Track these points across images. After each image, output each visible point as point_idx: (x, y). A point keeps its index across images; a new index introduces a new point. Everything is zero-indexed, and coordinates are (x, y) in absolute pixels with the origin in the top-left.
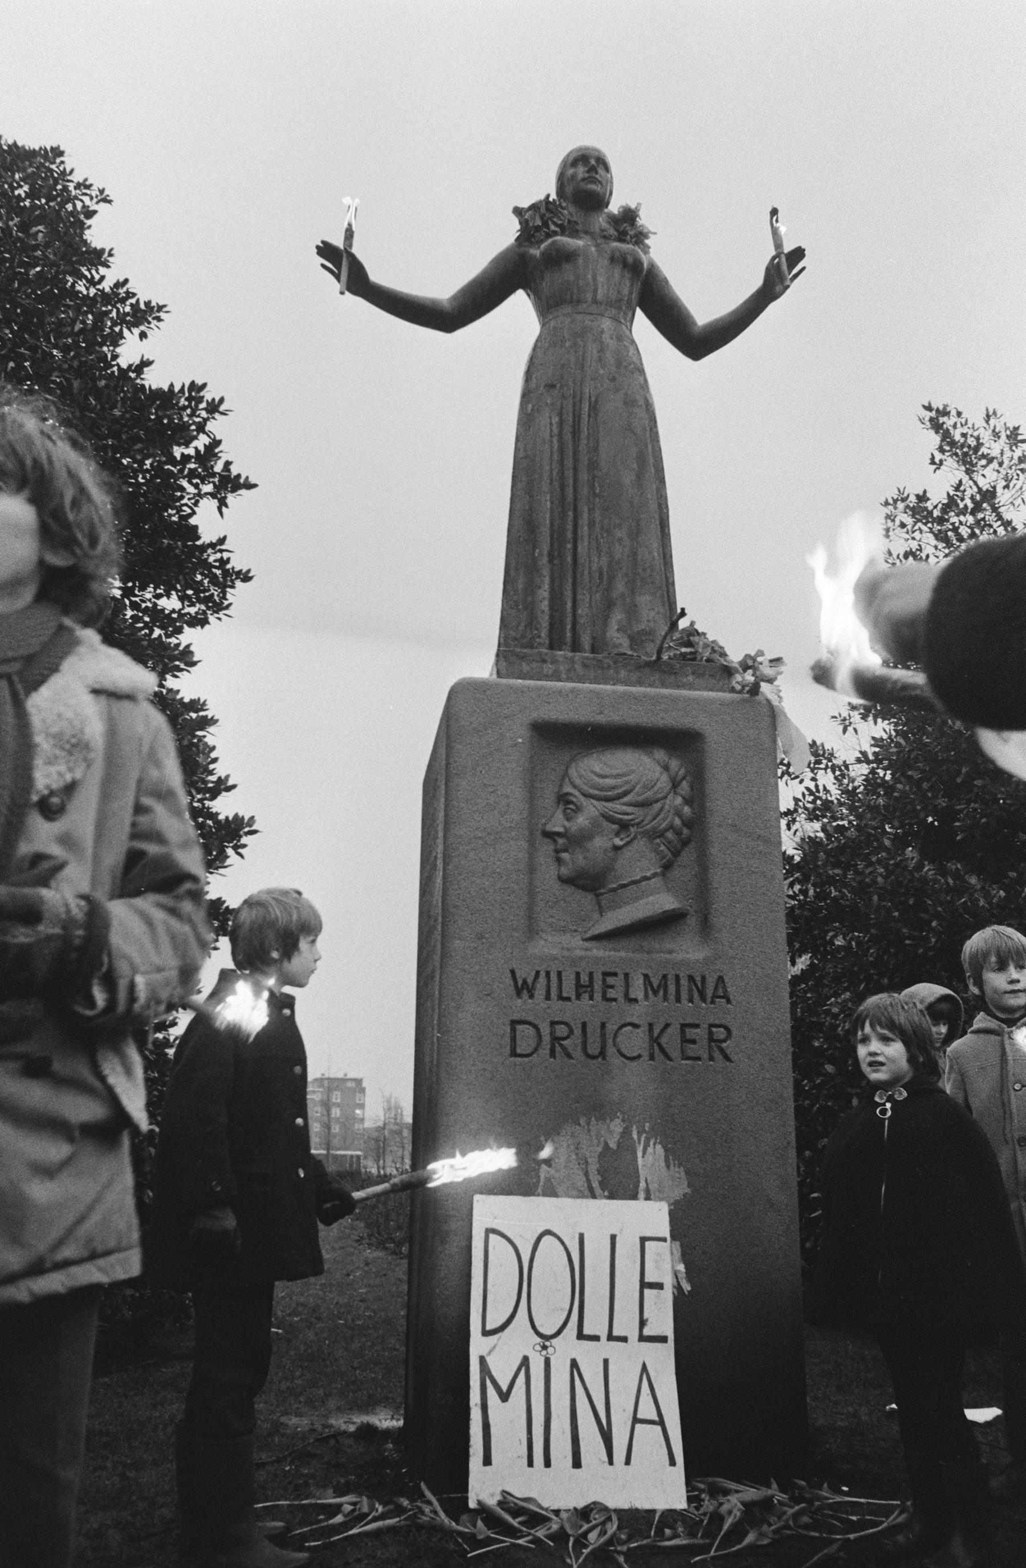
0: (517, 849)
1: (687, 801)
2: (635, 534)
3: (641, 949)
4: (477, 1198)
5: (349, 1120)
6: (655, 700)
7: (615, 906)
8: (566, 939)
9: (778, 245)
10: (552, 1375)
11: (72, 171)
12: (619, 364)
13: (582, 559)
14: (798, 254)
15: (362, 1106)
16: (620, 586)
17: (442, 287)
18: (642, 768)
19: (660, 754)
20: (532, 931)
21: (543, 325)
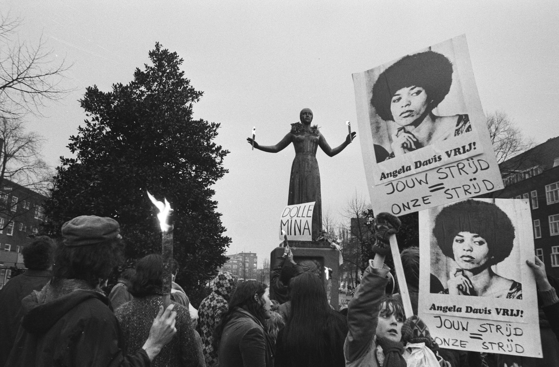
1: (320, 270)
5: (251, 268)
6: (314, 251)
9: (350, 131)
12: (312, 167)
14: (354, 133)
15: (256, 263)
19: (315, 261)
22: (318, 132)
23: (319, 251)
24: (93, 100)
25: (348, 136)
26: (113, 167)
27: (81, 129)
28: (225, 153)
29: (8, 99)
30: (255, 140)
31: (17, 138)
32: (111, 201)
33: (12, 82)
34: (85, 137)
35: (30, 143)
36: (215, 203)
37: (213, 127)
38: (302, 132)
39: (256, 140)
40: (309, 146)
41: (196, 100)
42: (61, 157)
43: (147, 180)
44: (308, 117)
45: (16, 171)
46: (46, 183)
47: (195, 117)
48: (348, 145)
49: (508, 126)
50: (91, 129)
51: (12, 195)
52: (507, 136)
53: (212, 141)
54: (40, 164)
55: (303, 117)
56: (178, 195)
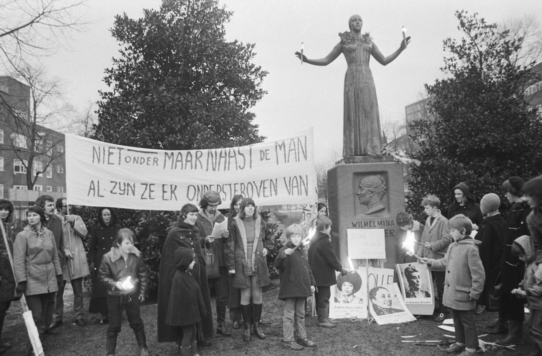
1: (385, 185)
2: (372, 123)
3: (376, 216)
9: (404, 37)
10: (373, 170)
11: (242, 43)
14: (409, 38)
16: (370, 137)
17: (323, 55)
19: (379, 176)
24: (124, 28)
25: (403, 41)
26: (154, 97)
27: (115, 60)
28: (263, 75)
29: (38, 34)
30: (304, 54)
33: (39, 16)
34: (120, 69)
36: (256, 126)
37: (248, 48)
38: (353, 40)
40: (361, 55)
41: (227, 20)
43: (190, 106)
44: (358, 23)
47: (228, 39)
48: (403, 52)
49: (538, 29)
52: (537, 40)
53: (251, 62)
54: (69, 108)
55: (353, 25)
56: (222, 120)
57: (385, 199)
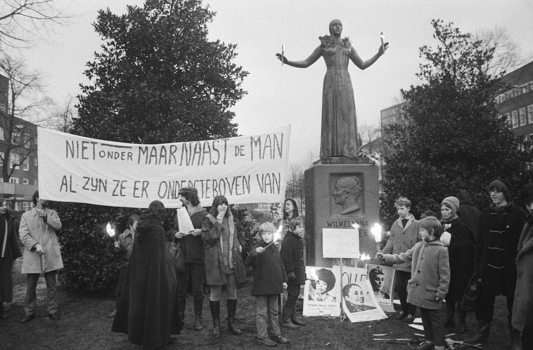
0: (328, 199)
1: (360, 186)
2: (349, 125)
4: (324, 257)
7: (346, 208)
8: (337, 215)
9: (382, 43)
11: (224, 43)
13: (338, 130)
14: (387, 44)
18: (352, 180)
19: (355, 177)
20: (331, 213)
21: (328, 70)
22: (349, 45)
23: (359, 166)
24: (106, 23)
25: (381, 47)
26: (135, 92)
27: (97, 55)
28: (244, 74)
30: (284, 55)
31: (22, 76)
32: (136, 127)
33: (20, 8)
35: (35, 80)
36: (235, 125)
37: (230, 48)
38: (333, 44)
39: (285, 55)
40: (340, 58)
41: (210, 20)
42: (80, 85)
44: (338, 28)
45: (26, 109)
46: (56, 118)
47: (210, 38)
49: (508, 41)
50: (108, 55)
51: (24, 132)
52: (507, 51)
53: (232, 62)
54: (48, 101)
55: (333, 29)
56: (202, 118)
57: (360, 200)
